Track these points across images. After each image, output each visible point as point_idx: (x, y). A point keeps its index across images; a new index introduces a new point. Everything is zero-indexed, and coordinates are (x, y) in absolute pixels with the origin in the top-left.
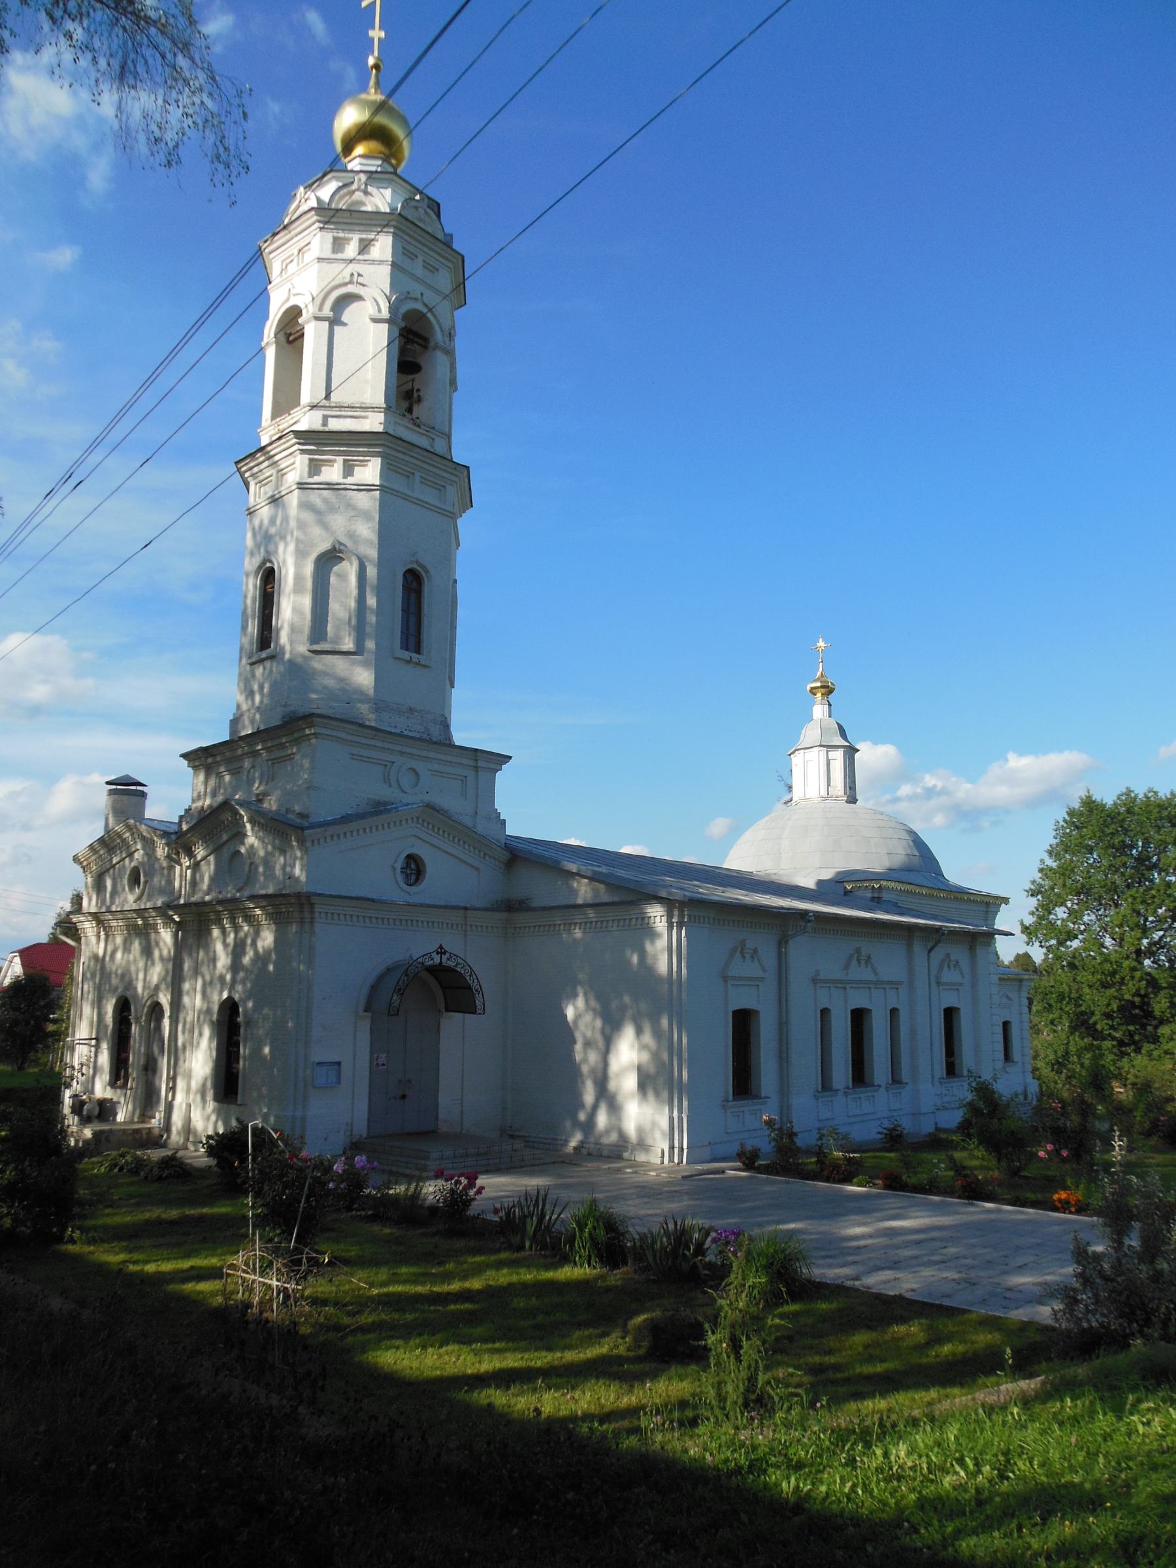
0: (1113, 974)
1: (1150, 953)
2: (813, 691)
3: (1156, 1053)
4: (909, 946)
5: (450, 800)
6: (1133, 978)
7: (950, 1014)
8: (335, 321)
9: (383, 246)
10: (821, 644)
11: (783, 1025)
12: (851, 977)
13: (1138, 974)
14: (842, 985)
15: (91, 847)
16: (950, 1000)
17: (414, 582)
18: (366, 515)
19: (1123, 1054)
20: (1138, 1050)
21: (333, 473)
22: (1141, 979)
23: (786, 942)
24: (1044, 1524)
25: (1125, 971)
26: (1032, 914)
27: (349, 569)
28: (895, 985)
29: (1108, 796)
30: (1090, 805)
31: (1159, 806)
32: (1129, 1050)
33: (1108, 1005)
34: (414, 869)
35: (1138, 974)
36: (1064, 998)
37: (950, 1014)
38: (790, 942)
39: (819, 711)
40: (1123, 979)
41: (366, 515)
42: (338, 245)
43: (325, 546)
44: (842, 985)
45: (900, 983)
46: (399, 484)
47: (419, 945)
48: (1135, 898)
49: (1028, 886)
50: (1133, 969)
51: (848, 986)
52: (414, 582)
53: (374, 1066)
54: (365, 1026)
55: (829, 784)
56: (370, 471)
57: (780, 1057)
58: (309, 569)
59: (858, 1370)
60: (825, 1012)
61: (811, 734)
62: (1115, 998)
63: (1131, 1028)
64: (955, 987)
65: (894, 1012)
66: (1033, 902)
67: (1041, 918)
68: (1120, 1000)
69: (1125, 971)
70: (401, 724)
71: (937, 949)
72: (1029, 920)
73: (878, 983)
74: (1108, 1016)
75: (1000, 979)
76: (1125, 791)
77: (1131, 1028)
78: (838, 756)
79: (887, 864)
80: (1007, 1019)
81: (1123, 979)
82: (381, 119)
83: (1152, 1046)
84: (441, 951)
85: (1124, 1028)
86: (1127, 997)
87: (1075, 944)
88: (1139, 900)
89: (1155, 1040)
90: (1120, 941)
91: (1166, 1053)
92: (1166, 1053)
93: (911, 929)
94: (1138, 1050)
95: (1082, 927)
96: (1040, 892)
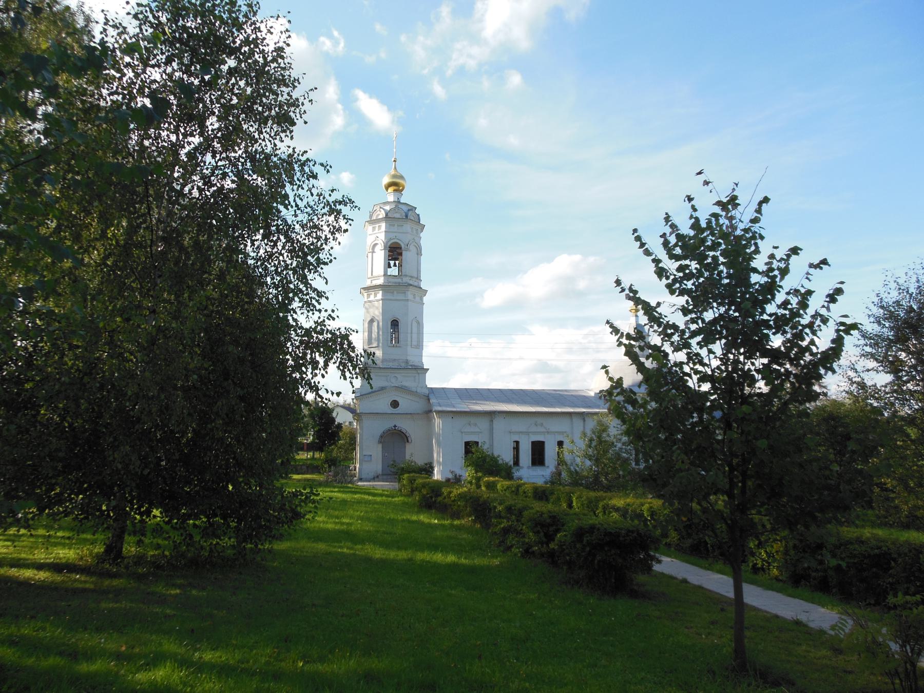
5: (409, 383)
8: (373, 252)
9: (383, 225)
15: (601, 391)
17: (395, 324)
18: (377, 308)
21: (372, 298)
24: (552, 558)
27: (375, 324)
34: (395, 404)
41: (377, 308)
42: (374, 229)
43: (369, 319)
46: (389, 296)
47: (387, 425)
52: (395, 324)
53: (383, 456)
54: (380, 446)
56: (380, 295)
58: (366, 325)
59: (72, 552)
60: (517, 443)
70: (391, 365)
82: (395, 180)
84: (395, 426)
93: (570, 414)
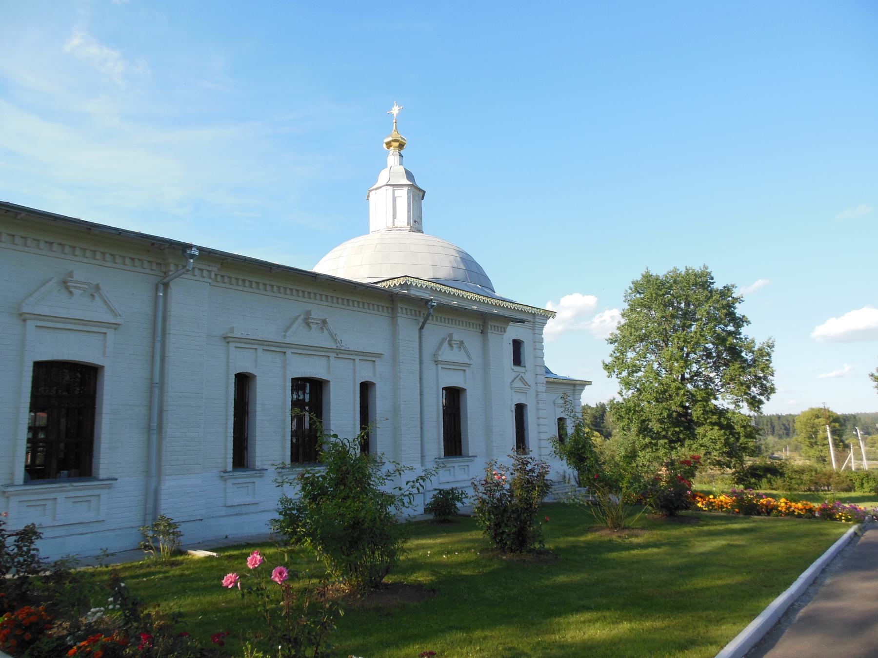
0: (665, 391)
1: (691, 380)
2: (389, 145)
3: (694, 446)
4: (394, 318)
6: (677, 394)
7: (454, 395)
10: (395, 110)
11: (156, 388)
12: (288, 340)
13: (682, 392)
14: (279, 348)
16: (454, 380)
19: (673, 448)
20: (682, 445)
22: (684, 395)
23: (166, 285)
25: (672, 390)
26: (611, 355)
28: (371, 357)
29: (660, 271)
30: (647, 278)
31: (695, 275)
32: (677, 445)
33: (661, 414)
35: (682, 392)
36: (630, 410)
37: (454, 395)
38: (172, 285)
39: (392, 159)
40: (670, 396)
44: (279, 348)
45: (379, 356)
48: (679, 339)
49: (608, 336)
50: (679, 388)
51: (289, 351)
55: (394, 216)
57: (149, 429)
60: (243, 381)
61: (383, 177)
62: (666, 409)
63: (677, 429)
64: (462, 367)
65: (366, 388)
66: (612, 347)
67: (617, 358)
68: (669, 410)
69: (672, 390)
71: (427, 326)
72: (609, 360)
73: (340, 352)
74: (661, 421)
75: (548, 382)
76: (672, 269)
77: (677, 429)
78: (403, 195)
79: (429, 276)
80: (522, 401)
81: (670, 396)
83: (692, 442)
85: (672, 429)
86: (674, 408)
87: (640, 374)
88: (682, 339)
89: (694, 436)
90: (670, 371)
91: (701, 446)
92: (701, 446)
94: (682, 445)
95: (645, 363)
96: (616, 341)
